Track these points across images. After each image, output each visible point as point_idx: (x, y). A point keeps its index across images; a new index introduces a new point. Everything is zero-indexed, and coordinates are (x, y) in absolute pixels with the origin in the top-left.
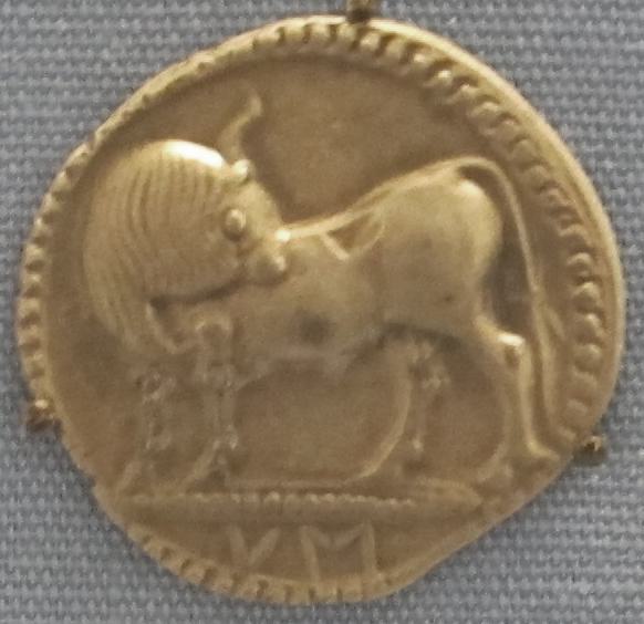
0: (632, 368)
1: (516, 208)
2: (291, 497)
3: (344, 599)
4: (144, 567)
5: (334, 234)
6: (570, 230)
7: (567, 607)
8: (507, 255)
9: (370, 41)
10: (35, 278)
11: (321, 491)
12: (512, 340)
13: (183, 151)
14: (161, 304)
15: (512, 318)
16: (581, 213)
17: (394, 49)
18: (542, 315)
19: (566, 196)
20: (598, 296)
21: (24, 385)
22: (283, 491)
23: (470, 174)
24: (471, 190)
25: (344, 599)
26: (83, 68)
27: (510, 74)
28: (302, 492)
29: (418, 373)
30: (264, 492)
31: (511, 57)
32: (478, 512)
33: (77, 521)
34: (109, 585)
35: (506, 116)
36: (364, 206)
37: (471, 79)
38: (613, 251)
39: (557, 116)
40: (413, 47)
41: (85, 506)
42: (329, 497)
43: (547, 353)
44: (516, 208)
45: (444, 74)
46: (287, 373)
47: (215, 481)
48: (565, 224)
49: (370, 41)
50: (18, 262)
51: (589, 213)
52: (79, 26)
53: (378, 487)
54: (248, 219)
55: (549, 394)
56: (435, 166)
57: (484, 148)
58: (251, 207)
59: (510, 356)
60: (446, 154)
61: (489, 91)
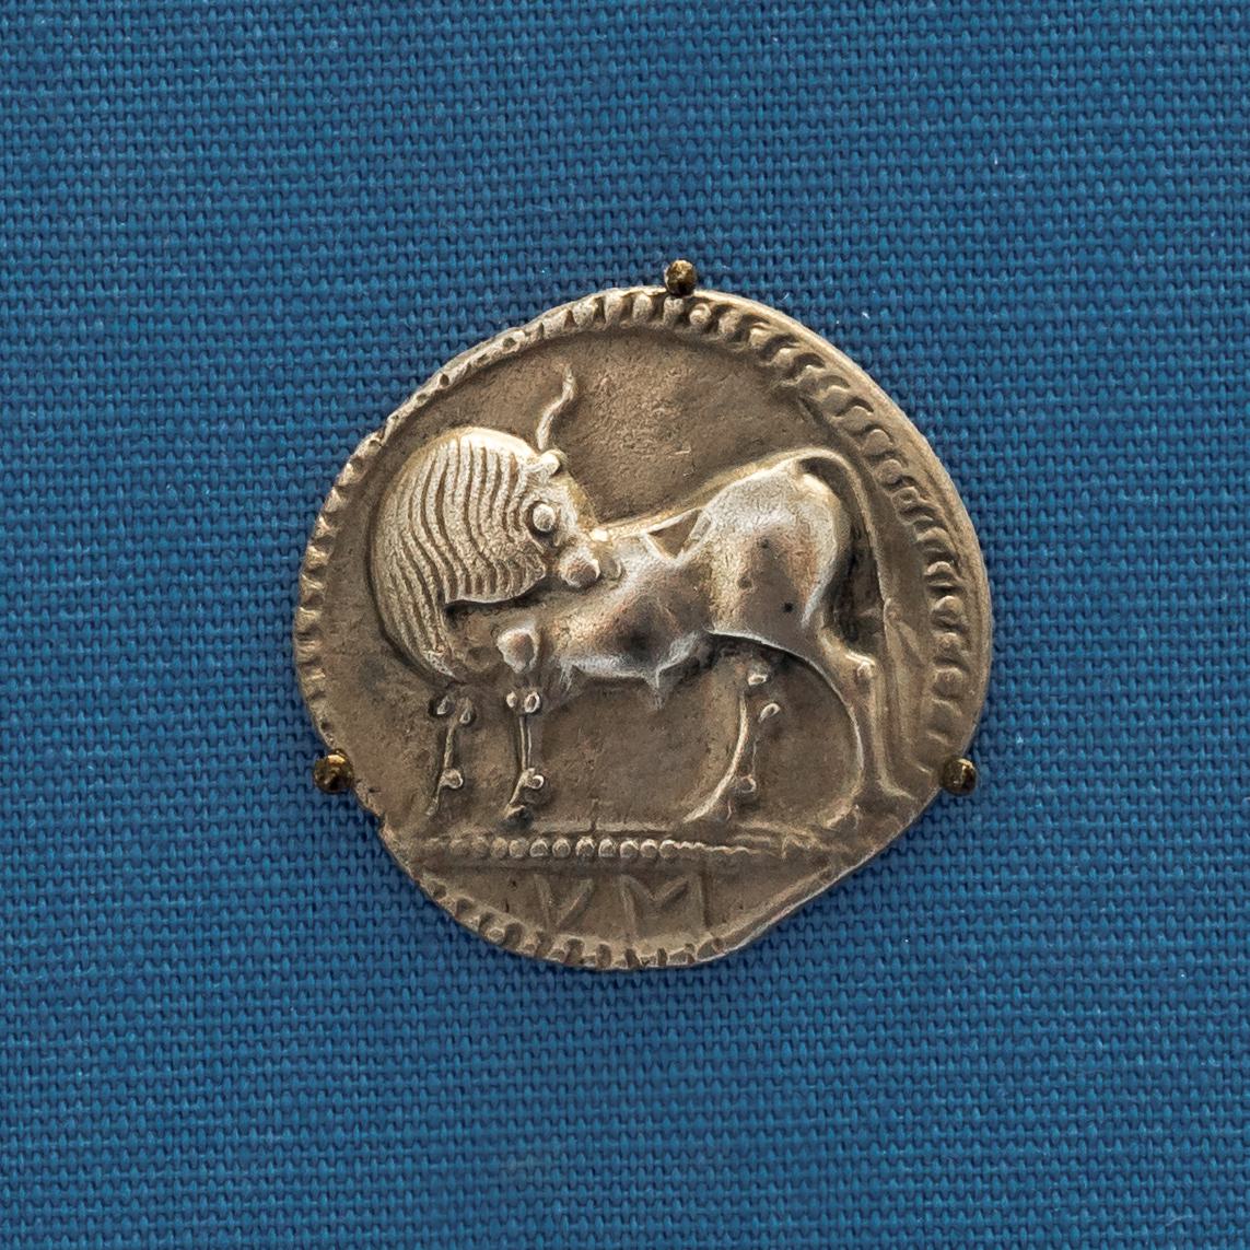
0: (986, 741)
1: (866, 512)
2: (606, 842)
3: (669, 962)
4: (464, 947)
5: (655, 534)
6: (930, 533)
7: (1225, 60)
8: (853, 568)
9: (700, 314)
10: (317, 585)
11: (640, 836)
12: (865, 662)
13: (478, 439)
14: (456, 612)
15: (857, 633)
16: (942, 513)
17: (727, 323)
18: (895, 633)
19: (924, 493)
20: (961, 610)
21: (315, 739)
22: (597, 837)
23: (812, 467)
24: (814, 486)
25: (669, 962)
26: (369, 371)
27: (857, 355)
28: (618, 837)
29: (754, 695)
30: (573, 837)
31: (856, 335)
32: (820, 860)
33: (385, 896)
34: (425, 971)
35: (857, 401)
36: (691, 504)
37: (814, 359)
38: (977, 558)
39: (912, 401)
40: (750, 320)
41: (393, 879)
42: (649, 843)
43: (901, 674)
44: (866, 512)
45: (785, 352)
46: (598, 687)
47: (521, 824)
48: (923, 526)
49: (700, 314)
50: (295, 567)
51: (950, 514)
52: (362, 323)
53: (712, 830)
54: (558, 515)
55: (905, 725)
56: (775, 457)
57: (831, 440)
58: (561, 502)
59: (862, 683)
60: (788, 444)
61: (838, 372)
